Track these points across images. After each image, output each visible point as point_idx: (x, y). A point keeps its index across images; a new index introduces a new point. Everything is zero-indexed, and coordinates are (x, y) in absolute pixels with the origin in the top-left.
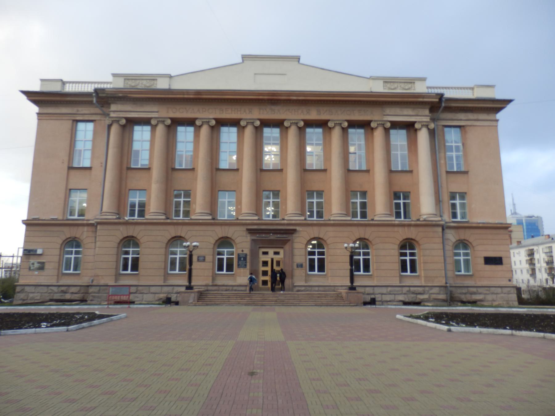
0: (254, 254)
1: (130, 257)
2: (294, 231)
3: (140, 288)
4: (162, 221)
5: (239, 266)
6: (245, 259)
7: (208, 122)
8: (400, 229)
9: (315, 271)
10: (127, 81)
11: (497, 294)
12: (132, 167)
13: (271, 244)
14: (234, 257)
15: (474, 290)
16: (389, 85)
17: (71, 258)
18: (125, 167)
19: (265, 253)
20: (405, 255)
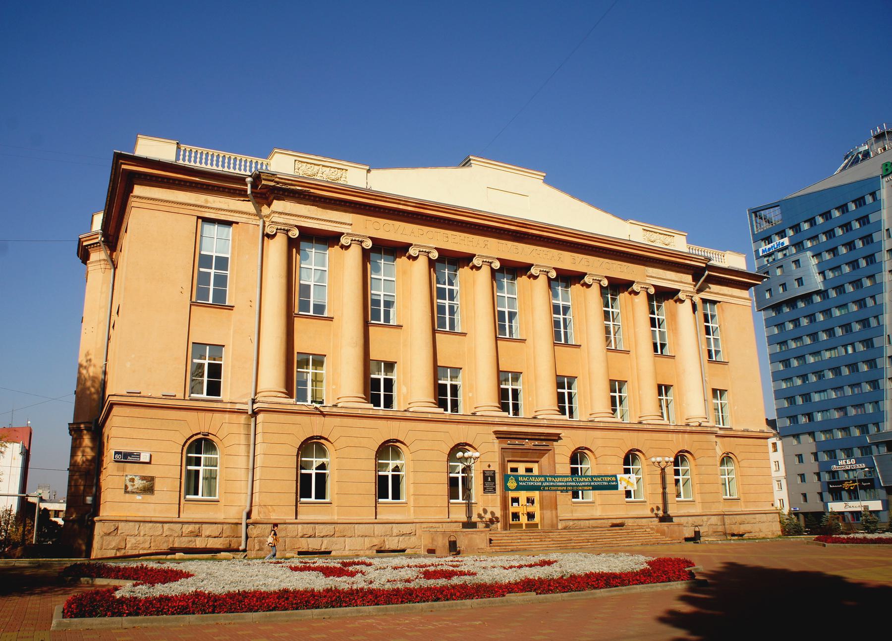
1: (201, 469)
2: (558, 437)
3: (121, 525)
7: (362, 242)
10: (298, 165)
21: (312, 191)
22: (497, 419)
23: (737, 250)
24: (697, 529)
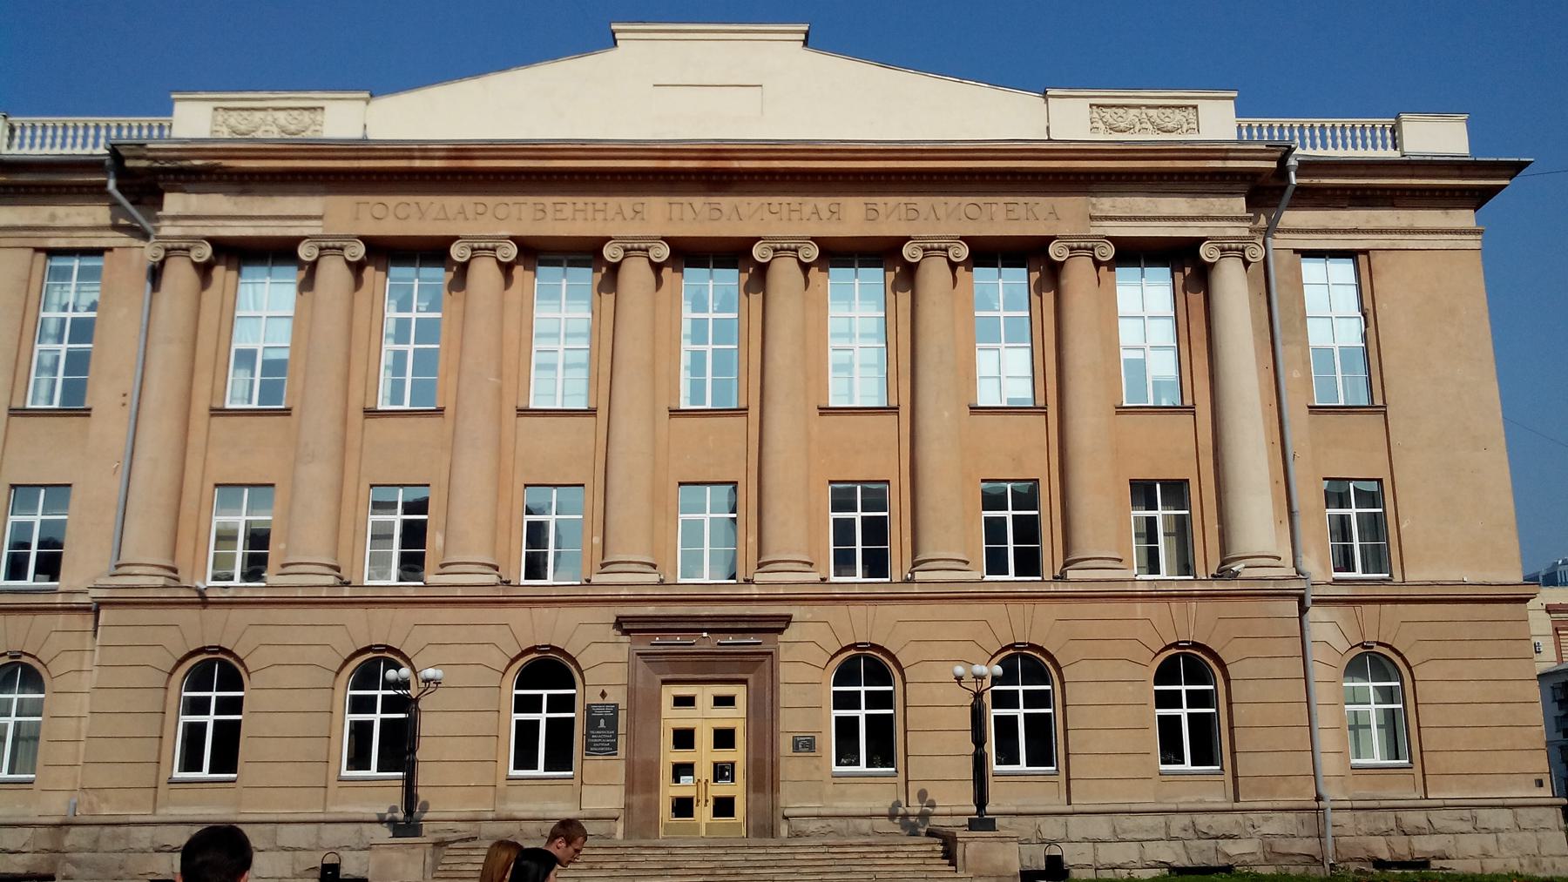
0: (644, 706)
4: (324, 593)
5: (588, 747)
6: (612, 723)
7: (494, 249)
8: (1155, 609)
9: (369, 768)
10: (221, 116)
11: (1497, 831)
12: (228, 406)
13: (705, 668)
14: (578, 715)
15: (1417, 818)
16: (1108, 114)
17: (371, 723)
18: (201, 406)
19: (685, 702)
20: (200, 706)
21: (225, 163)
22: (625, 591)
23: (1438, 108)
24: (1055, 851)
